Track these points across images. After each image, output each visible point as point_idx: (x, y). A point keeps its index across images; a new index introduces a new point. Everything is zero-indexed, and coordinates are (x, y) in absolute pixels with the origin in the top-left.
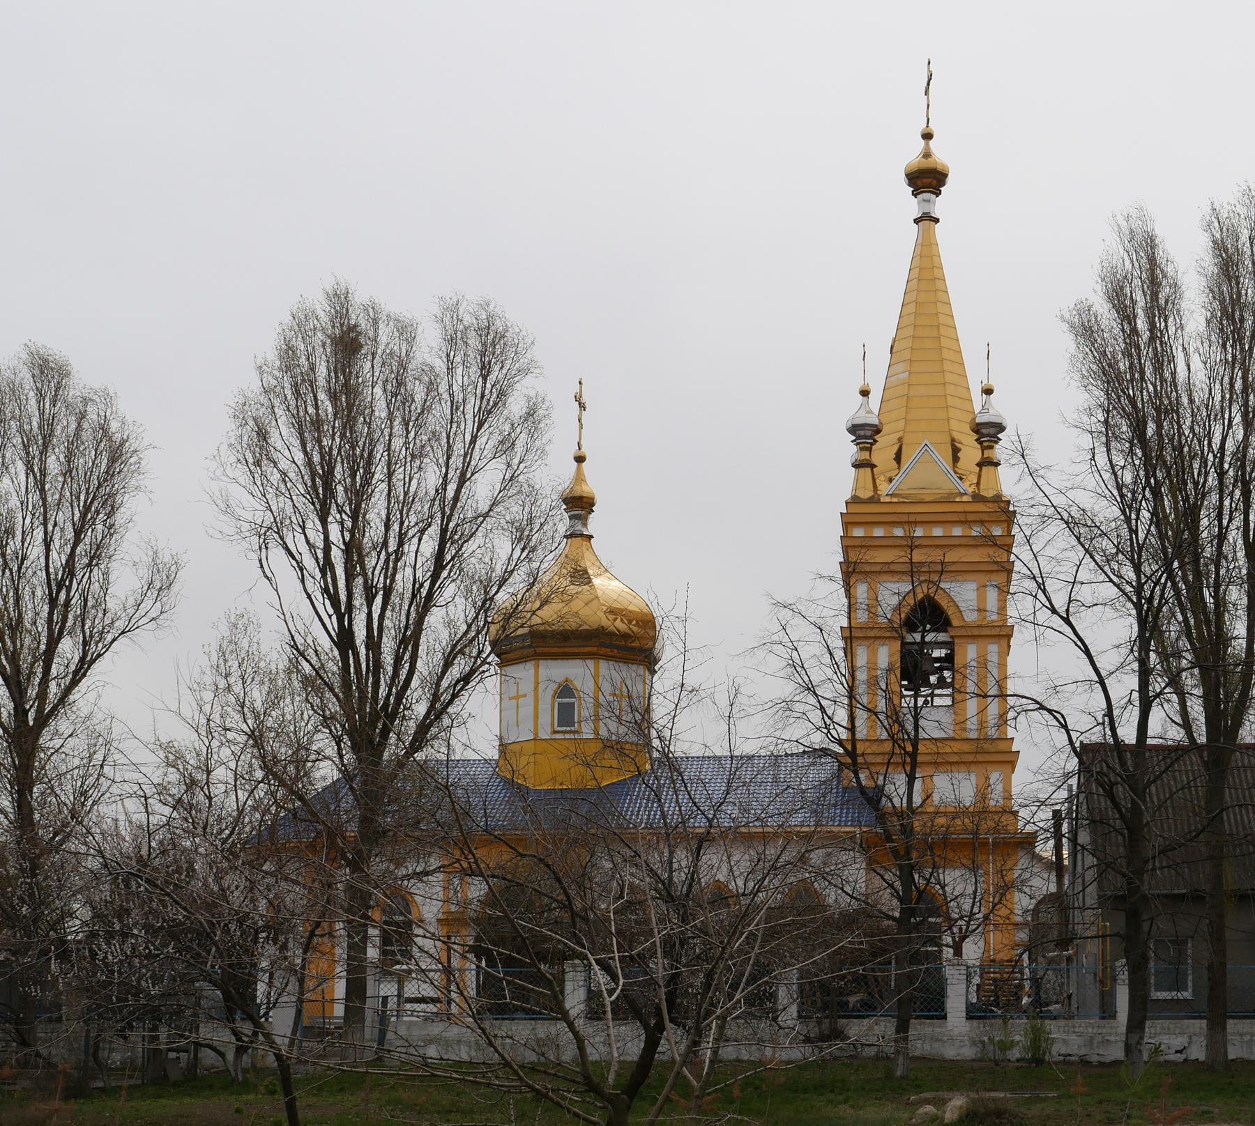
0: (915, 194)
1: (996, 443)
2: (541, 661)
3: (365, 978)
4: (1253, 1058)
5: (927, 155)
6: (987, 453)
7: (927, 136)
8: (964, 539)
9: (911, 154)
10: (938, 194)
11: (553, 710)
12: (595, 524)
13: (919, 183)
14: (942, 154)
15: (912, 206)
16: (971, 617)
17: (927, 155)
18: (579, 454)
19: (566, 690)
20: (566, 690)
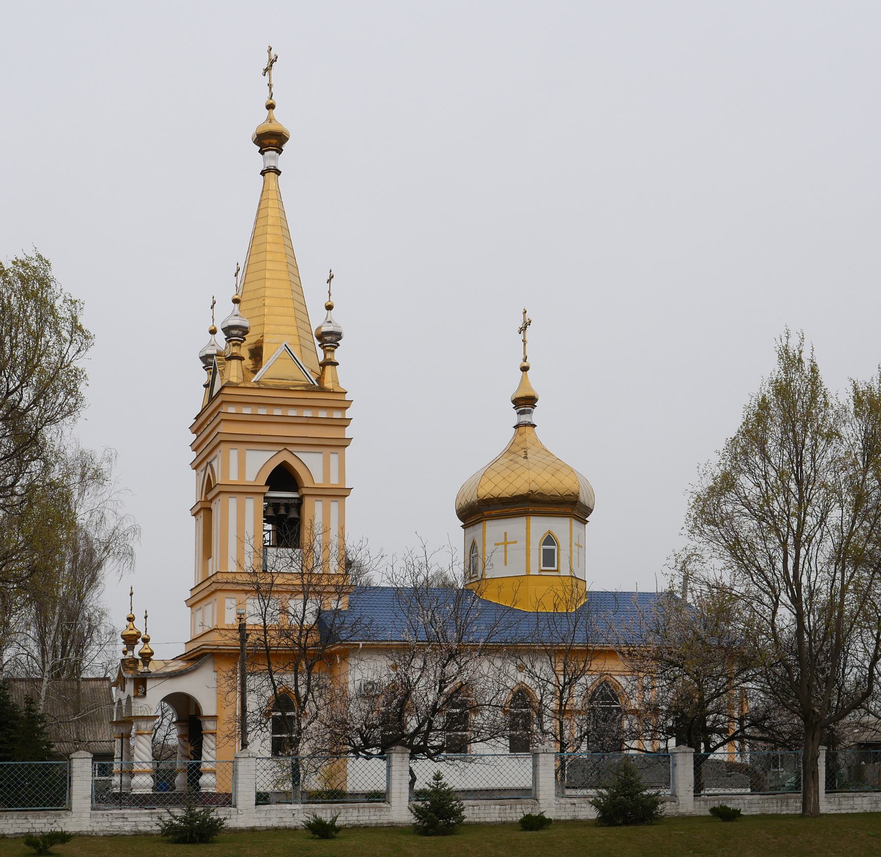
0: (262, 152)
1: (336, 347)
2: (531, 518)
3: (273, 733)
4: (880, 810)
5: (270, 120)
6: (329, 356)
7: (270, 107)
8: (328, 420)
9: (258, 120)
10: (279, 151)
11: (540, 553)
12: (536, 415)
13: (266, 142)
14: (283, 120)
15: (258, 161)
16: (319, 480)
17: (270, 120)
18: (525, 364)
19: (549, 540)
20: (549, 540)
